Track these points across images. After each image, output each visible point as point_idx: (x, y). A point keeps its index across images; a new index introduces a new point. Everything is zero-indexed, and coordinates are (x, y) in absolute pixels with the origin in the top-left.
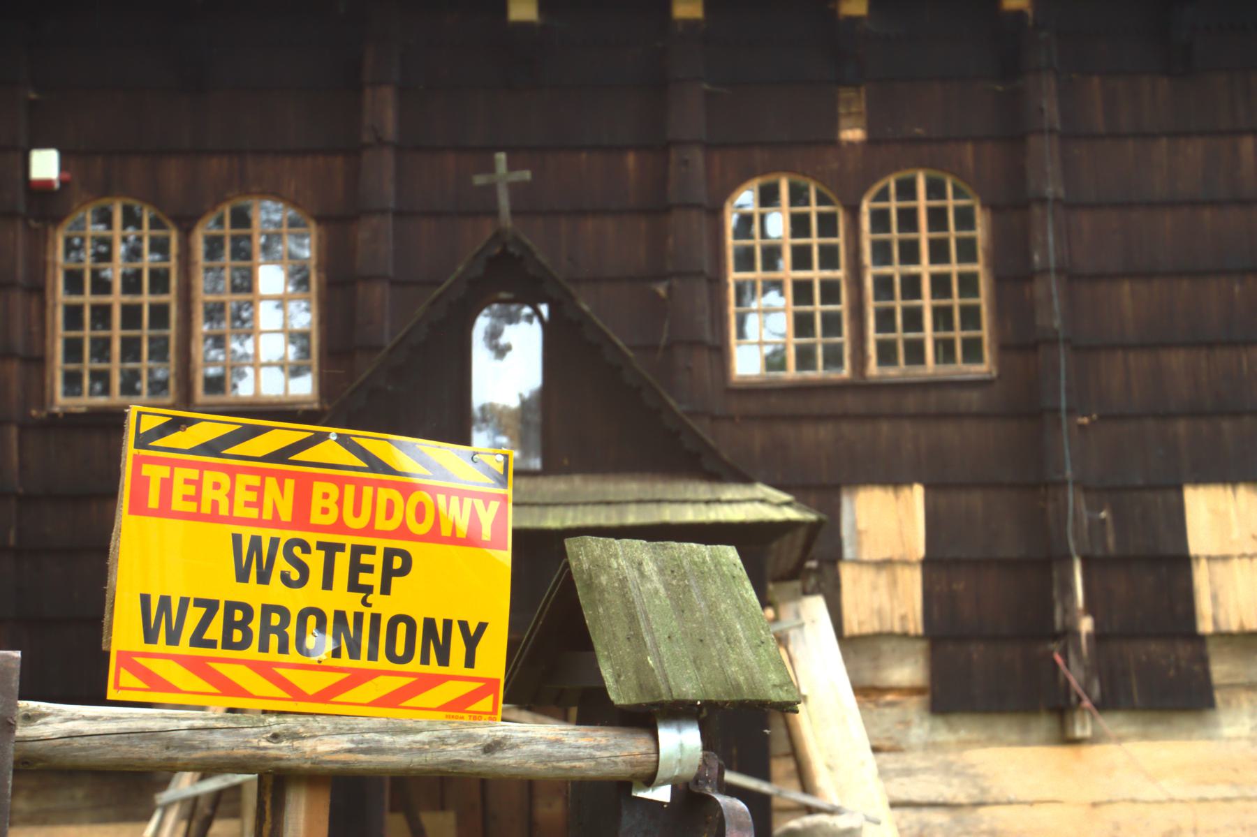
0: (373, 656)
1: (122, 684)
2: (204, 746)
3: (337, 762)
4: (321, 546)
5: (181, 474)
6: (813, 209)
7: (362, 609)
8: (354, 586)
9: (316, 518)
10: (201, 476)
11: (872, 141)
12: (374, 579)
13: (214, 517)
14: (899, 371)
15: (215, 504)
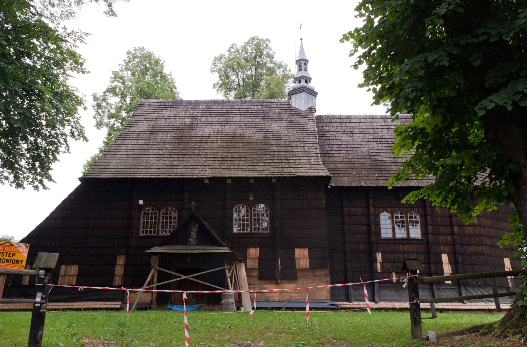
8: (9, 256)
9: (5, 250)
11: (254, 200)
12: (11, 256)
14: (145, 234)
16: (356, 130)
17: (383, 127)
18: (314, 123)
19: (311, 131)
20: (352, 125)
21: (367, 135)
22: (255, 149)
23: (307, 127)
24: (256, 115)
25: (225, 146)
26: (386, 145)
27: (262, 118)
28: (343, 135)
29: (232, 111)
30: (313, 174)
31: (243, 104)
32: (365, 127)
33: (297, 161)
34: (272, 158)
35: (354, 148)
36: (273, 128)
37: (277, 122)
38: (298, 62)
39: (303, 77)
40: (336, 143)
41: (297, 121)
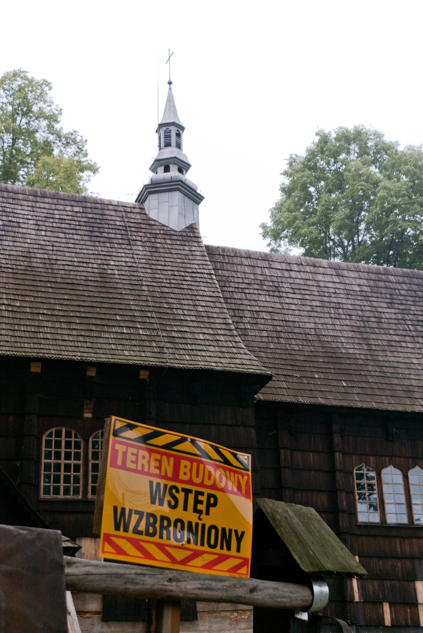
0: (202, 544)
1: (105, 550)
2: (141, 583)
3: (193, 594)
4: (183, 490)
5: (131, 450)
6: (73, 439)
7: (198, 521)
8: (196, 510)
9: (182, 477)
10: (138, 452)
11: (93, 418)
12: (202, 507)
13: (142, 472)
15: (143, 466)
16: (285, 285)
17: (338, 286)
18: (203, 258)
19: (202, 276)
20: (274, 273)
21: (308, 297)
22: (86, 299)
23: (192, 266)
24: (72, 227)
25: (11, 286)
26: (347, 322)
27: (87, 233)
28: (261, 292)
29: (16, 211)
30: (232, 368)
31: (39, 199)
32: (302, 282)
33: (189, 336)
34: (130, 325)
35: (286, 321)
36: (116, 259)
37: (123, 246)
38: (164, 129)
39: (175, 160)
40: (249, 308)
41: (167, 251)
